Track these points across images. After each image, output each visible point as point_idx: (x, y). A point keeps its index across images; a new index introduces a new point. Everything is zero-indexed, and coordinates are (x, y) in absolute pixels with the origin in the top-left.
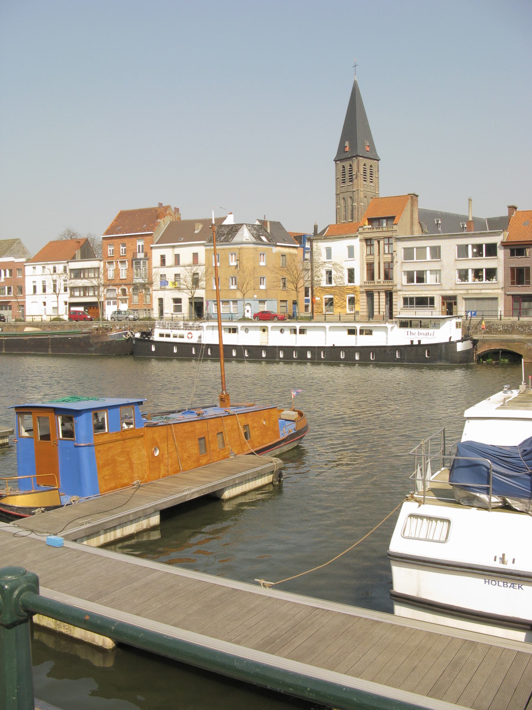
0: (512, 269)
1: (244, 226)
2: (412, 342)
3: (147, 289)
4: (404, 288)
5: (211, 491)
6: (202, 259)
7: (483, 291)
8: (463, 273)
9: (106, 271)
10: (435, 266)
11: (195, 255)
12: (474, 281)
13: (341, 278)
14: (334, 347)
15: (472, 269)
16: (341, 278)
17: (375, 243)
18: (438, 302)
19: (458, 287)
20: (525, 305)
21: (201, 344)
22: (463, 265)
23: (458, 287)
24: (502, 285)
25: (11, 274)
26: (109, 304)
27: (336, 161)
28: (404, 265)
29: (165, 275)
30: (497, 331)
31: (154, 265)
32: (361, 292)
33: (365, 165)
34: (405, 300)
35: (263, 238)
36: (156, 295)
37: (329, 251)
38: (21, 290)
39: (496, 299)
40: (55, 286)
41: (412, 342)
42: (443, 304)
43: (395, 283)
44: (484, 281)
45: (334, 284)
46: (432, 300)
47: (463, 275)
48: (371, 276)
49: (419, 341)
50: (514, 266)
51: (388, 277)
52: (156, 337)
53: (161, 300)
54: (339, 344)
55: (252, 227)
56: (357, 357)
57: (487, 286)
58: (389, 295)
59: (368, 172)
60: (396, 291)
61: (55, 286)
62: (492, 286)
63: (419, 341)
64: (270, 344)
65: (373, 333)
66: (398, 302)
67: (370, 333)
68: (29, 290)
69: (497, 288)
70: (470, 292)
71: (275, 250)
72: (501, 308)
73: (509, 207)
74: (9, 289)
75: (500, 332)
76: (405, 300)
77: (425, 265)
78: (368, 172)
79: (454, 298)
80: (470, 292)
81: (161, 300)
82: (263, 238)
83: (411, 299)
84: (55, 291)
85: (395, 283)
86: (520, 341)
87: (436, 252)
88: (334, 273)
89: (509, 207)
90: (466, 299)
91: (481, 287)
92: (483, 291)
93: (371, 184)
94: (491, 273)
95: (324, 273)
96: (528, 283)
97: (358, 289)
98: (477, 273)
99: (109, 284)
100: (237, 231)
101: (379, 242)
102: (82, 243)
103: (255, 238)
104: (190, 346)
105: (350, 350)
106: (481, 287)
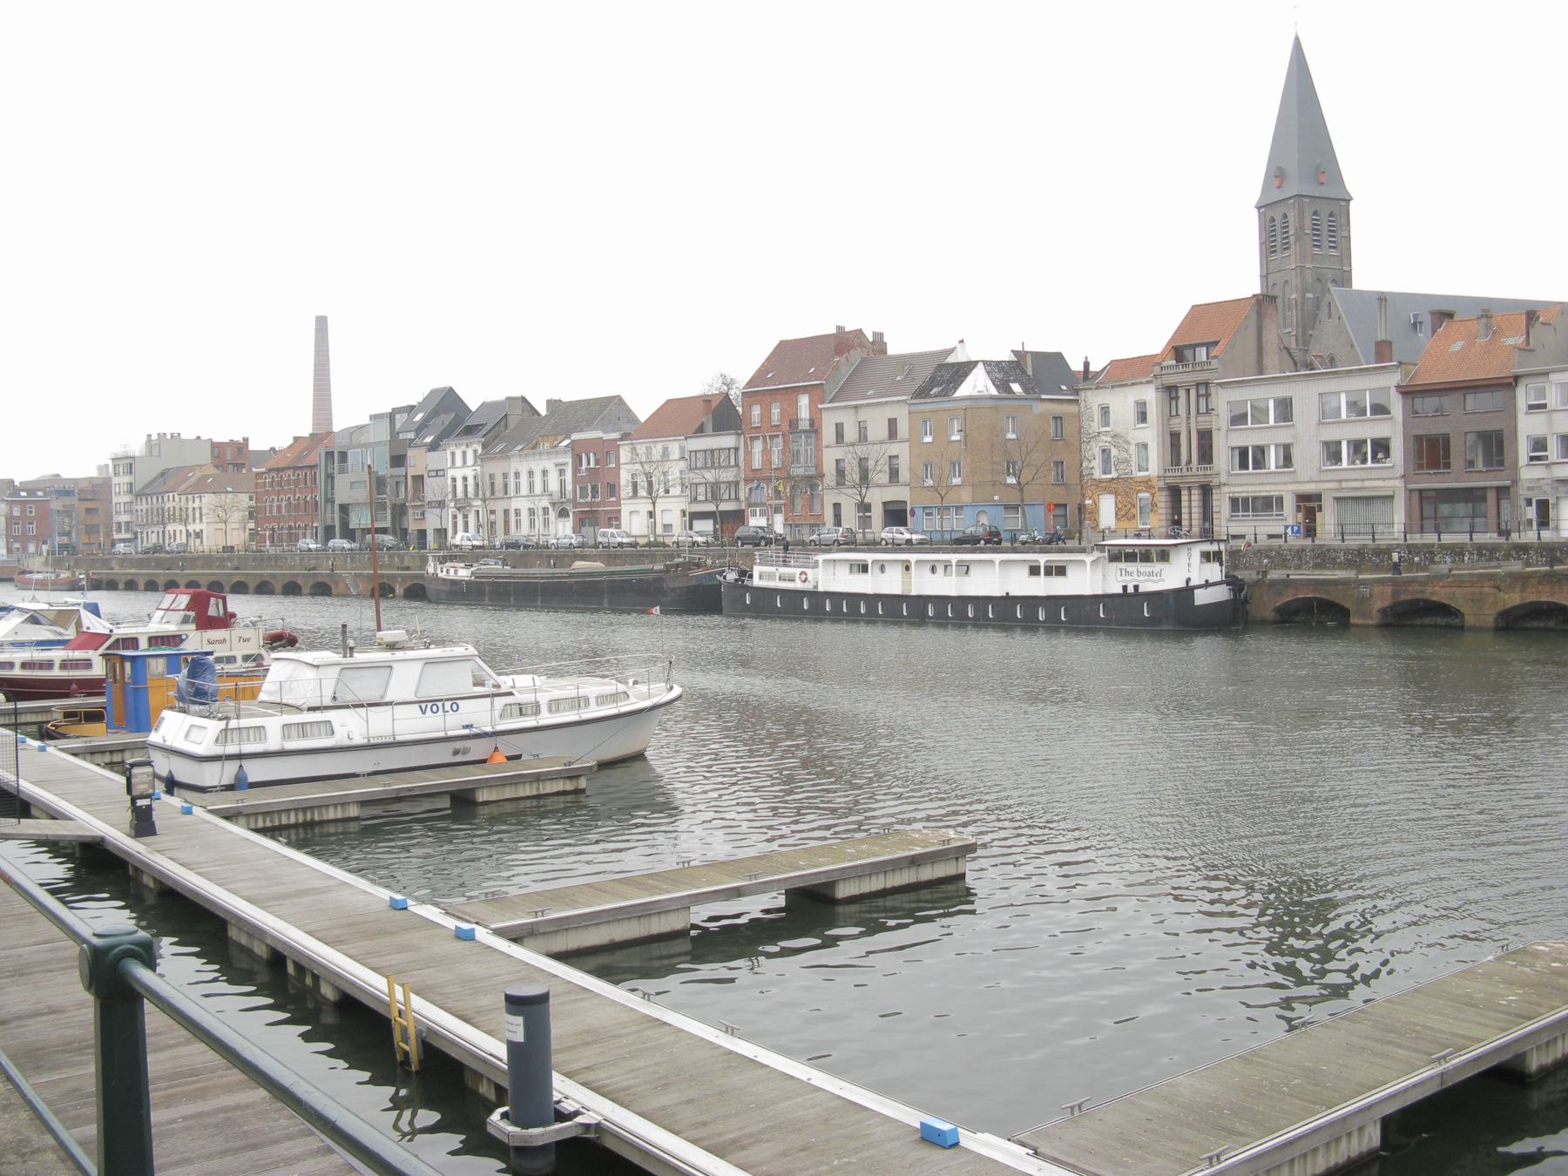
0: (1418, 438)
1: (980, 366)
2: (1125, 588)
3: (813, 487)
4: (1232, 480)
5: (463, 787)
6: (903, 429)
7: (1367, 484)
8: (1333, 449)
9: (748, 453)
10: (1284, 436)
11: (892, 423)
12: (1353, 463)
13: (1127, 461)
14: (1007, 597)
15: (1277, 446)
16: (1127, 461)
17: (1182, 393)
18: (1289, 504)
19: (1324, 477)
20: (1445, 509)
21: (817, 593)
22: (1331, 434)
23: (1324, 477)
24: (1400, 471)
25: (597, 462)
26: (754, 514)
27: (1259, 208)
28: (1232, 435)
29: (837, 461)
30: (1335, 565)
31: (825, 443)
32: (1160, 489)
33: (1315, 213)
34: (1234, 502)
35: (1016, 388)
36: (829, 499)
37: (1105, 411)
38: (613, 489)
39: (1391, 497)
40: (650, 484)
41: (1125, 588)
42: (1298, 509)
43: (1216, 470)
44: (1369, 464)
45: (1114, 475)
46: (1280, 499)
47: (1332, 452)
48: (1176, 460)
49: (1136, 587)
50: (1420, 432)
51: (1206, 455)
52: (756, 582)
53: (837, 506)
54: (1016, 591)
55: (993, 367)
56: (1041, 617)
57: (1374, 474)
58: (1206, 491)
59: (1324, 227)
60: (1219, 486)
61: (650, 484)
62: (1384, 474)
63: (1136, 587)
64: (913, 593)
65: (1069, 571)
66: (1221, 505)
67: (1061, 571)
68: (626, 491)
69: (1390, 477)
70: (1344, 485)
71: (1039, 408)
72: (1399, 518)
73: (1433, 313)
74: (594, 489)
75: (1341, 566)
76: (1234, 502)
77: (1270, 436)
78: (1324, 227)
79: (1317, 497)
80: (1344, 485)
81: (837, 506)
82: (1016, 388)
83: (1246, 500)
84: (650, 493)
85: (1216, 470)
86: (1345, 583)
87: (1285, 409)
88: (1114, 452)
89: (1433, 313)
90: (1338, 499)
91: (1363, 475)
92: (1367, 484)
93: (1333, 252)
94: (1381, 447)
95: (1097, 452)
96: (1447, 466)
97: (1154, 483)
98: (1357, 446)
99: (756, 478)
100: (966, 375)
101: (1188, 391)
102: (714, 405)
103: (997, 387)
104: (799, 594)
105: (1031, 602)
106: (1363, 475)
